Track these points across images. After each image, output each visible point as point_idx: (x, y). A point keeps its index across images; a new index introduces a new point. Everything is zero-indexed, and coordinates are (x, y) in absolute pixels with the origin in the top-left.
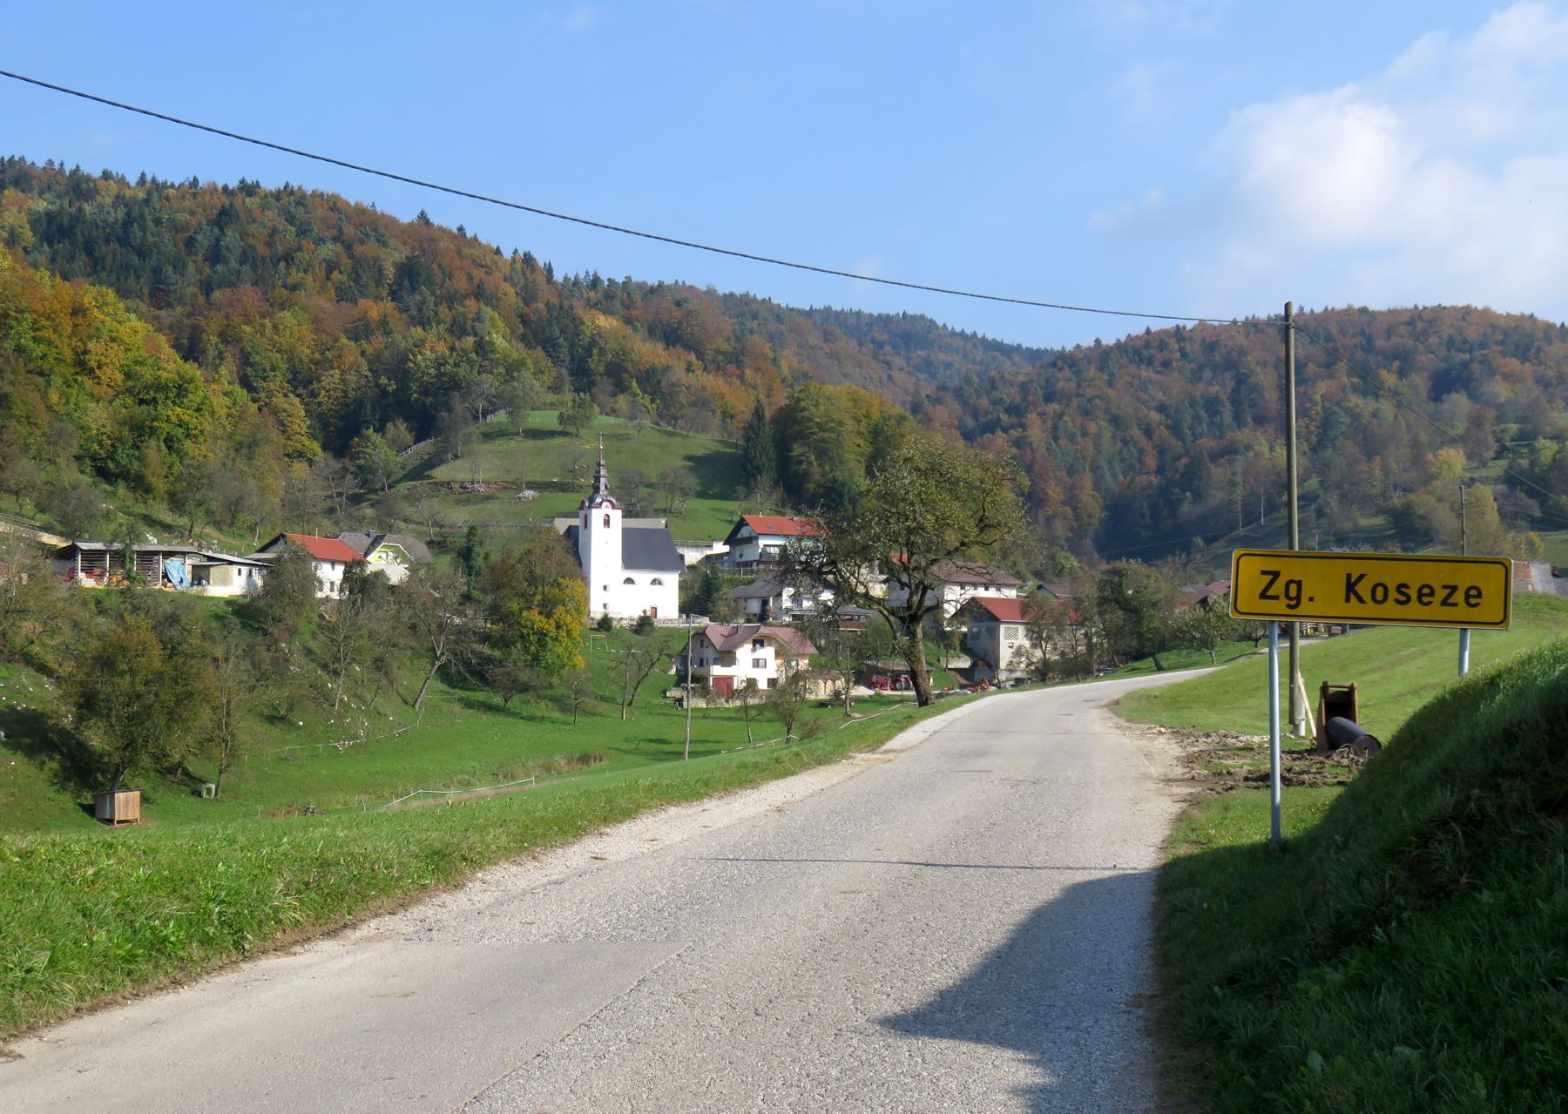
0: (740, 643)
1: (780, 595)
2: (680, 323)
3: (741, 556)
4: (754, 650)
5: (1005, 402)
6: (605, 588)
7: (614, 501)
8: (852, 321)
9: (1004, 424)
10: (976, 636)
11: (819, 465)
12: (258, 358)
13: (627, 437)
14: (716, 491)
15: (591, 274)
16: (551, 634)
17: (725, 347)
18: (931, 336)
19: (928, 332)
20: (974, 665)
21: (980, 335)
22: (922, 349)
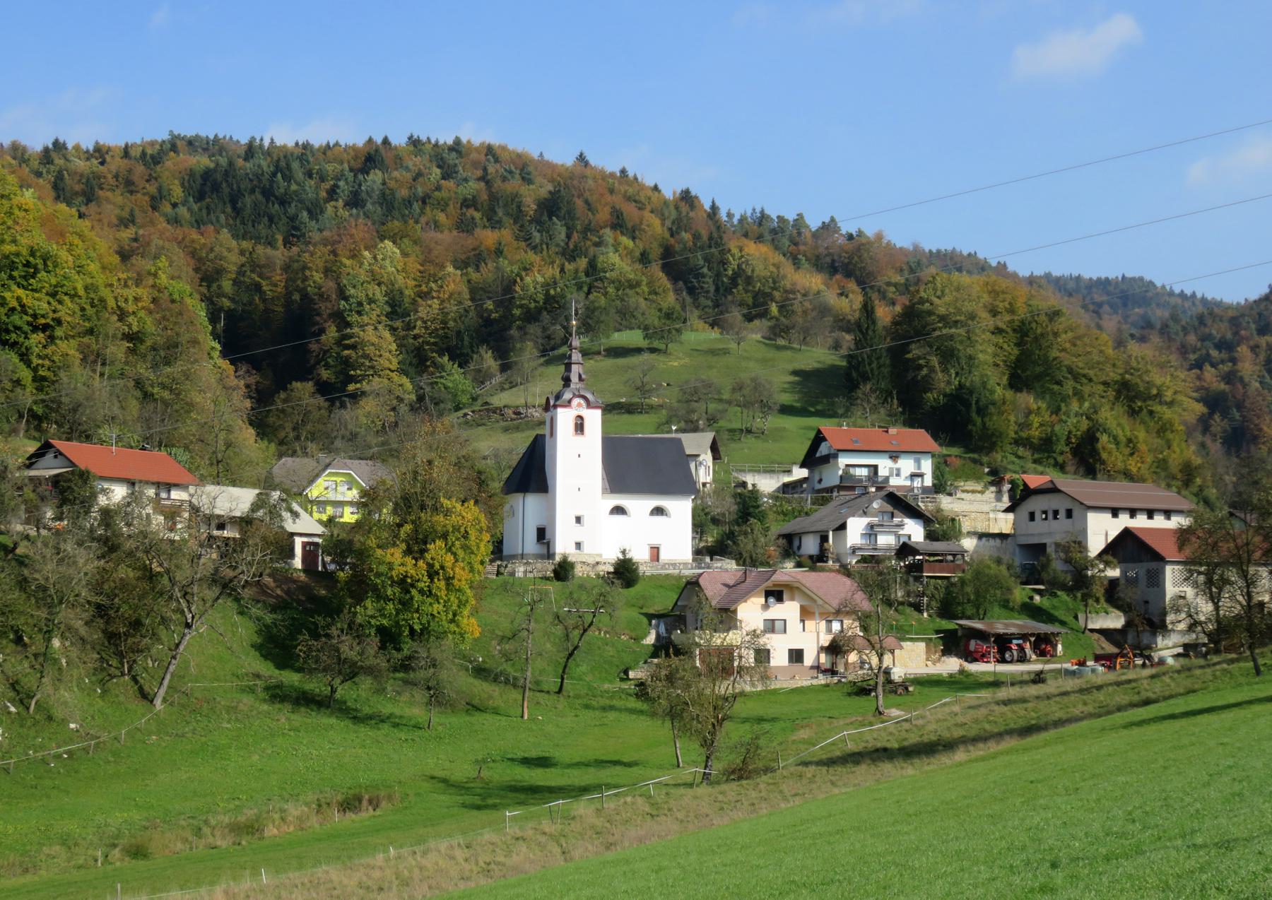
0: (744, 597)
1: (843, 527)
2: (851, 258)
3: (820, 481)
4: (766, 606)
5: (1215, 338)
6: (578, 520)
7: (590, 396)
8: (1071, 285)
9: (1214, 360)
10: (1132, 582)
11: (943, 371)
12: (352, 291)
13: (726, 352)
14: (819, 407)
15: (758, 210)
16: (421, 585)
17: (898, 279)
18: (1150, 294)
19: (1146, 291)
20: (1128, 624)
21: (1199, 295)
22: (1140, 306)
